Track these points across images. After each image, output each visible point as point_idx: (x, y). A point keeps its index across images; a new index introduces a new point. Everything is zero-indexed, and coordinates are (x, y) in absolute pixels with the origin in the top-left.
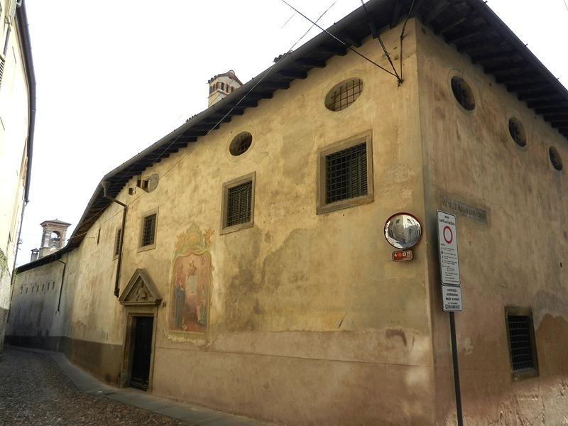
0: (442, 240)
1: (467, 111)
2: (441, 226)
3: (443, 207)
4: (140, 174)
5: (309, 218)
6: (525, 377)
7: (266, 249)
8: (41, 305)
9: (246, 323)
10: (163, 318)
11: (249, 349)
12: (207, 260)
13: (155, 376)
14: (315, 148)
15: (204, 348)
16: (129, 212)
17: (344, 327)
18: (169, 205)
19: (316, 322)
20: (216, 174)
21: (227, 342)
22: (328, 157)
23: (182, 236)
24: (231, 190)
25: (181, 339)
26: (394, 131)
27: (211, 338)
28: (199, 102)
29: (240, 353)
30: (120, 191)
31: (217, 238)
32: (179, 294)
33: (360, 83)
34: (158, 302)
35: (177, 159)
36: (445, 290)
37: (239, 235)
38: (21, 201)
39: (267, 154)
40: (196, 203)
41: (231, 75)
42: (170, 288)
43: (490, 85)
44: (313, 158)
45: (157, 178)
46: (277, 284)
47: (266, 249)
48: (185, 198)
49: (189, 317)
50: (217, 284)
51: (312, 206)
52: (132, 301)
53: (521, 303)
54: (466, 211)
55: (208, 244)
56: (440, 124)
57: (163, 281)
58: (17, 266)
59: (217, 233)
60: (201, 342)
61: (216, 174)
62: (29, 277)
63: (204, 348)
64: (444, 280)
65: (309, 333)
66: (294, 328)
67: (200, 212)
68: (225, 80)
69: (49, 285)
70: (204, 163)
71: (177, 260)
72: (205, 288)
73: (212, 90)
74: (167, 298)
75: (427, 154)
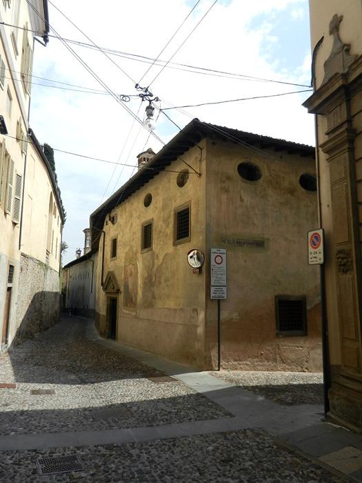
0: (213, 263)
1: (252, 182)
2: (213, 256)
3: (222, 244)
4: (110, 212)
5: (170, 249)
6: (286, 336)
7: (158, 262)
8: (83, 288)
9: (149, 304)
10: (121, 299)
11: (150, 318)
12: (136, 268)
13: (119, 332)
14: (173, 209)
15: (136, 317)
16: (106, 236)
17: (180, 307)
18: (121, 234)
19: (171, 304)
20: (139, 217)
21: (143, 313)
22: (178, 213)
23: (126, 253)
24: (146, 227)
25: (128, 312)
26: (198, 203)
27: (138, 312)
28: (130, 171)
29: (148, 320)
30: (147, 182)
31: (139, 255)
32: (126, 286)
33: (145, 206)
34: (118, 291)
35: (124, 206)
36: (212, 289)
37: (147, 254)
38: (56, 221)
39: (157, 208)
40: (131, 234)
41: (150, 151)
42: (123, 283)
43: (281, 157)
44: (172, 213)
45: (116, 214)
46: (160, 283)
47: (158, 262)
48: (127, 230)
49: (130, 301)
50: (140, 282)
51: (171, 242)
52: (108, 291)
53: (292, 290)
54: (245, 243)
55: (136, 259)
56: (224, 197)
57: (120, 277)
58: (65, 263)
59: (139, 252)
60: (134, 314)
61: (139, 217)
62: (72, 271)
63: (136, 317)
64: (212, 284)
65: (169, 309)
66: (165, 307)
67: (133, 239)
68: (145, 156)
69: (84, 276)
70: (135, 209)
71: (125, 266)
72: (135, 284)
73: (140, 161)
74: (122, 289)
75: (210, 216)
